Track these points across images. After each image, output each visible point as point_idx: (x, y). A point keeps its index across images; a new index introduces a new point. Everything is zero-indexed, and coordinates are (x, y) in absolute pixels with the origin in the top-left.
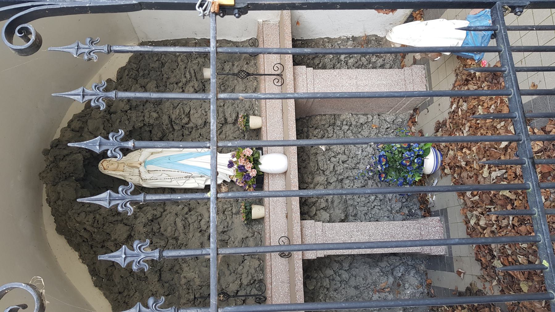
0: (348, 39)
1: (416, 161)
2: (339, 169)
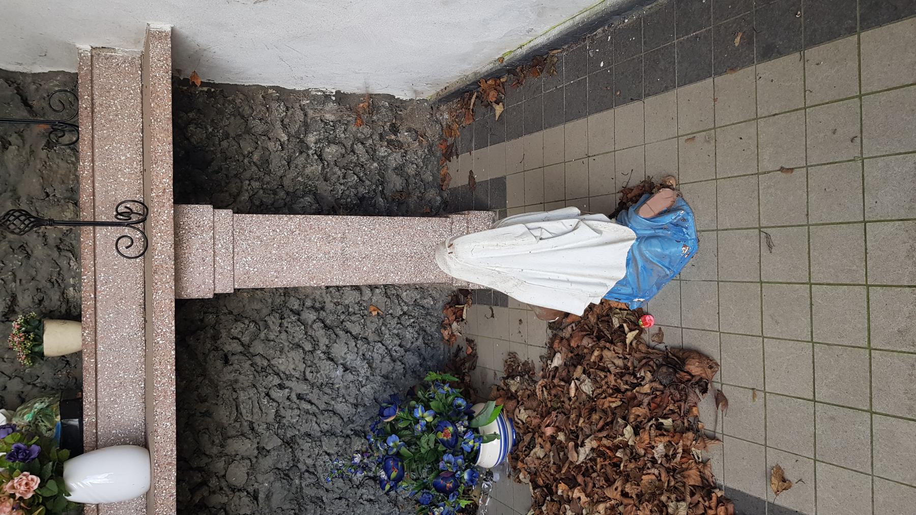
0: (327, 97)
1: (461, 429)
2: (291, 417)
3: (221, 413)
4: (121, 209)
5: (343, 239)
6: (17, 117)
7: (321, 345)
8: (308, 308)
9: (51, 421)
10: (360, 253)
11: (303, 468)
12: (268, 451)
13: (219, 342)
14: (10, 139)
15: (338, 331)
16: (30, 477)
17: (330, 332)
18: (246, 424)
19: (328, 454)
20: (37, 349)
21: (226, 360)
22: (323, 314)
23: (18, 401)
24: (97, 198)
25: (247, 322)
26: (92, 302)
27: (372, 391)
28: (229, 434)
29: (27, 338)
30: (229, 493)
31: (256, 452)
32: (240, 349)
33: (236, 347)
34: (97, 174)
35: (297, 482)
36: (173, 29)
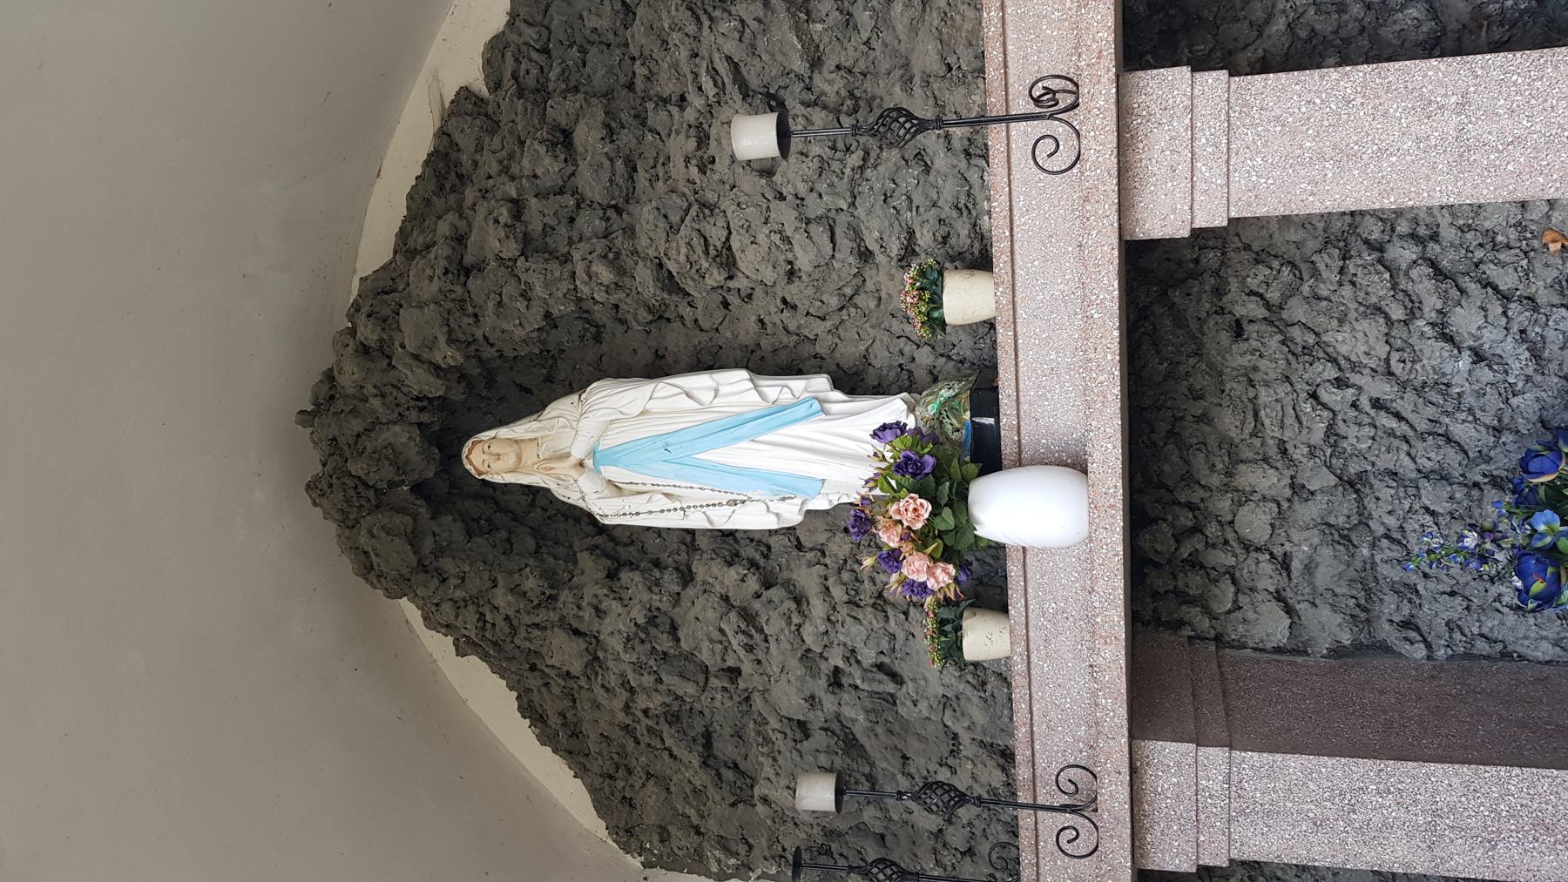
2: (1356, 437)
3: (1227, 420)
5: (1461, 106)
7: (1426, 310)
8: (1401, 237)
10: (1501, 132)
11: (1380, 531)
12: (1312, 493)
13: (1225, 299)
15: (1467, 283)
16: (920, 501)
17: (1448, 284)
18: (1271, 442)
19: (1432, 513)
20: (936, 314)
21: (1238, 331)
22: (1433, 249)
23: (929, 379)
24: (1011, 71)
25: (1276, 264)
27: (1537, 406)
28: (1244, 457)
30: (1238, 551)
31: (1288, 492)
32: (1261, 312)
33: (1254, 309)
35: (1365, 552)
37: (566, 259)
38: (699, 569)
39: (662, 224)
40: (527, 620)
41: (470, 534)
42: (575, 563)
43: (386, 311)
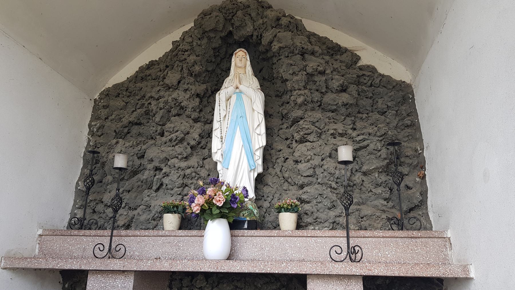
4: (357, 249)
6: (402, 205)
9: (248, 216)
14: (390, 202)
16: (223, 202)
20: (283, 210)
24: (362, 239)
26: (306, 235)
29: (288, 205)
34: (376, 239)
36: (471, 279)
37: (305, 88)
38: (199, 125)
39: (315, 120)
40: (185, 66)
41: (214, 49)
42: (203, 83)
43: (291, 28)
